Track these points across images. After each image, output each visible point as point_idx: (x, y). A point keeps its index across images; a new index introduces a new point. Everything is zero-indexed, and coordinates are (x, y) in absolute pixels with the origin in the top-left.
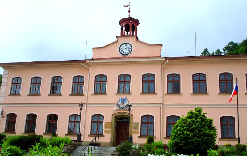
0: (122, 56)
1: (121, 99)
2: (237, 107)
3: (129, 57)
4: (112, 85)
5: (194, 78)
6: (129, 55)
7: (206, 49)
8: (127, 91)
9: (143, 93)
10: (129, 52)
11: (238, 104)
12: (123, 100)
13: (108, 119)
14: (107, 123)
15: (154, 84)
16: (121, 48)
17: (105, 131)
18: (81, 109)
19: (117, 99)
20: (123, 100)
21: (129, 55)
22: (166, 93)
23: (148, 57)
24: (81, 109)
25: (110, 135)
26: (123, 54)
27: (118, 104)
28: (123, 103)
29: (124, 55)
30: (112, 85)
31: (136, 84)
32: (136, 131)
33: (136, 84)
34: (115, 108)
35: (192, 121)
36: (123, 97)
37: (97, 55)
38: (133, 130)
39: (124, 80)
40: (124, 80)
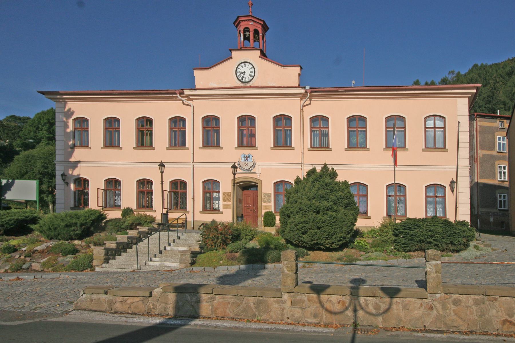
0: (240, 84)
1: (243, 156)
2: (393, 169)
3: (251, 87)
4: (228, 132)
5: (427, 123)
6: (251, 84)
8: (439, 145)
9: (313, 147)
10: (251, 78)
11: (457, 166)
12: (247, 158)
13: (226, 187)
14: (225, 194)
15: (403, 133)
17: (224, 205)
18: (162, 173)
20: (247, 158)
21: (251, 84)
22: (309, 146)
24: (162, 173)
25: (264, 191)
26: (242, 82)
28: (247, 162)
29: (244, 83)
30: (228, 132)
31: (265, 132)
32: (267, 206)
33: (265, 132)
36: (247, 152)
37: (202, 83)
38: (263, 204)
40: (246, 123)
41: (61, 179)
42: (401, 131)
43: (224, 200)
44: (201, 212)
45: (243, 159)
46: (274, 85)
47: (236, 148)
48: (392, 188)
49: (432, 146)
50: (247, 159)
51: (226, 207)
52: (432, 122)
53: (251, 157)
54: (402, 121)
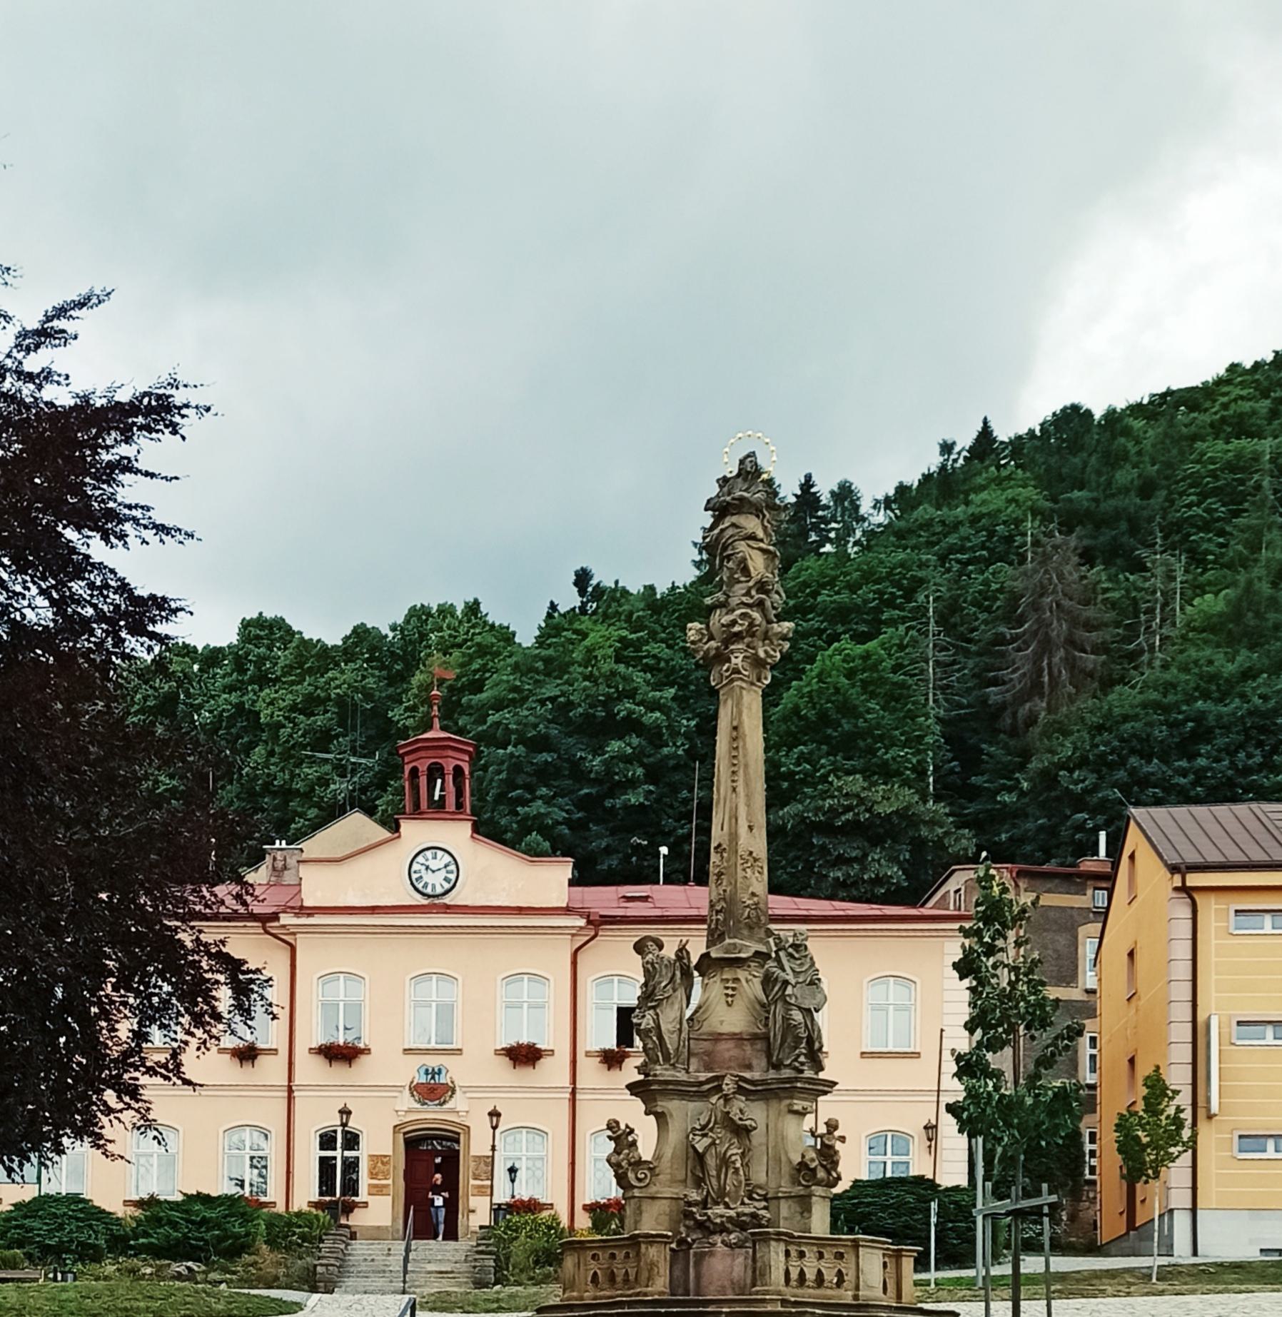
1: (422, 1071)
10: (447, 886)
13: (379, 1141)
14: (374, 1158)
21: (447, 900)
29: (429, 896)
34: (407, 1101)
51: (377, 1190)
53: (444, 1072)
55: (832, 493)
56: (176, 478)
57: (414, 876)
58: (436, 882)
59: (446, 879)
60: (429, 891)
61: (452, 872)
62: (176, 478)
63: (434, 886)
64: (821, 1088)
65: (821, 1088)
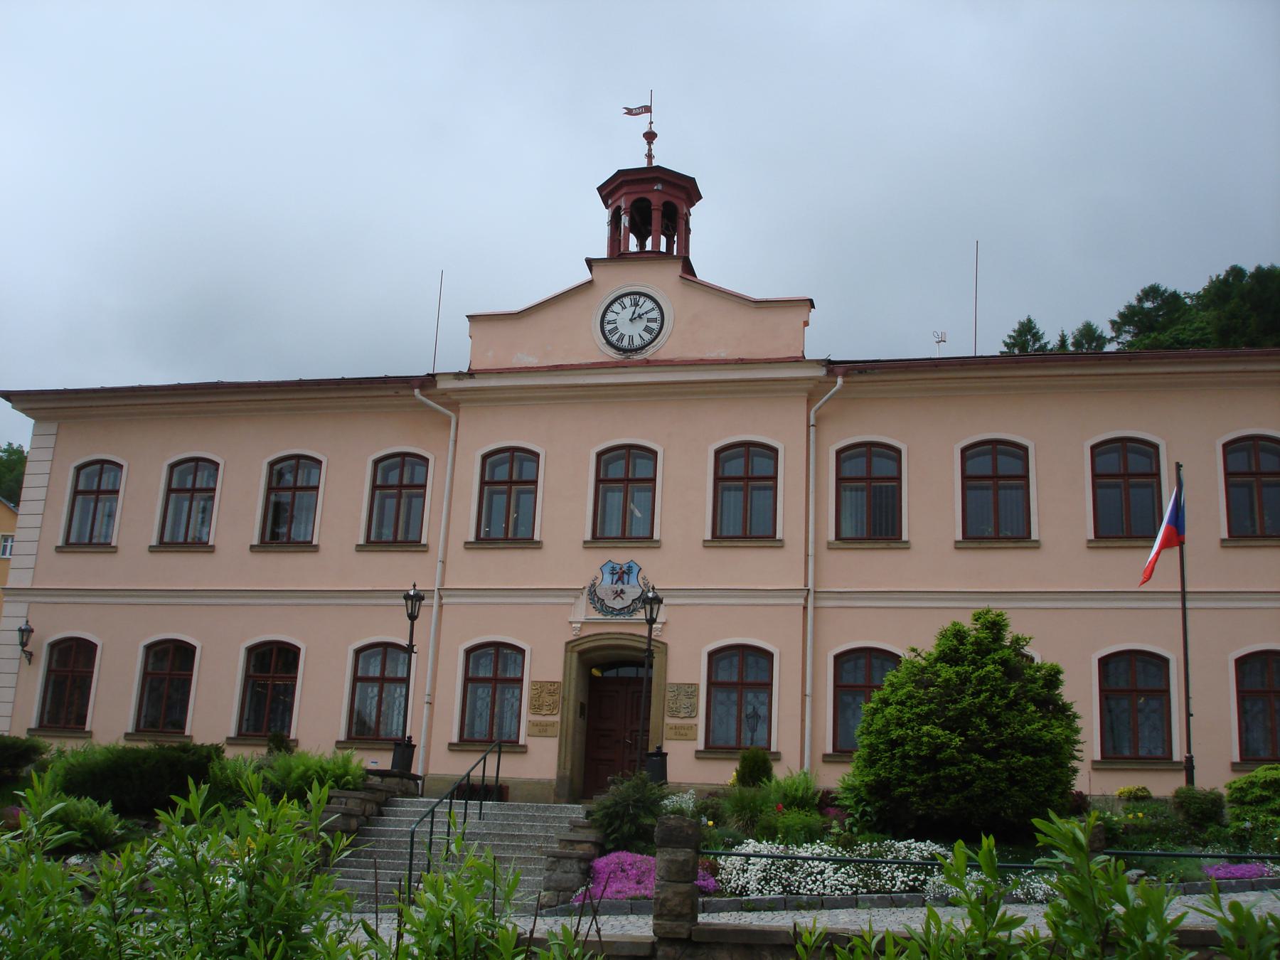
0: (612, 355)
1: (607, 569)
2: (1179, 605)
3: (648, 363)
4: (565, 500)
6: (648, 354)
7: (1029, 321)
10: (647, 337)
13: (546, 664)
14: (539, 686)
16: (610, 316)
17: (533, 724)
18: (413, 617)
19: (589, 567)
20: (621, 574)
21: (648, 354)
22: (832, 536)
23: (741, 362)
24: (413, 617)
27: (592, 592)
28: (619, 586)
29: (625, 351)
30: (565, 500)
31: (684, 495)
32: (682, 727)
33: (684, 495)
34: (582, 611)
35: (958, 674)
36: (621, 557)
39: (625, 477)
40: (625, 477)
41: (17, 641)
42: (1017, 488)
43: (536, 708)
44: (452, 747)
45: (608, 578)
46: (723, 354)
47: (958, 546)
48: (736, 660)
49: (388, 534)
50: (620, 579)
51: (540, 730)
52: (741, 461)
53: (635, 570)
54: (769, 458)
55: (1113, 323)
56: (630, 112)
57: (608, 327)
58: (633, 332)
59: (647, 329)
60: (625, 343)
61: (654, 320)
62: (630, 112)
63: (631, 338)
64: (1257, 517)
65: (1257, 517)
